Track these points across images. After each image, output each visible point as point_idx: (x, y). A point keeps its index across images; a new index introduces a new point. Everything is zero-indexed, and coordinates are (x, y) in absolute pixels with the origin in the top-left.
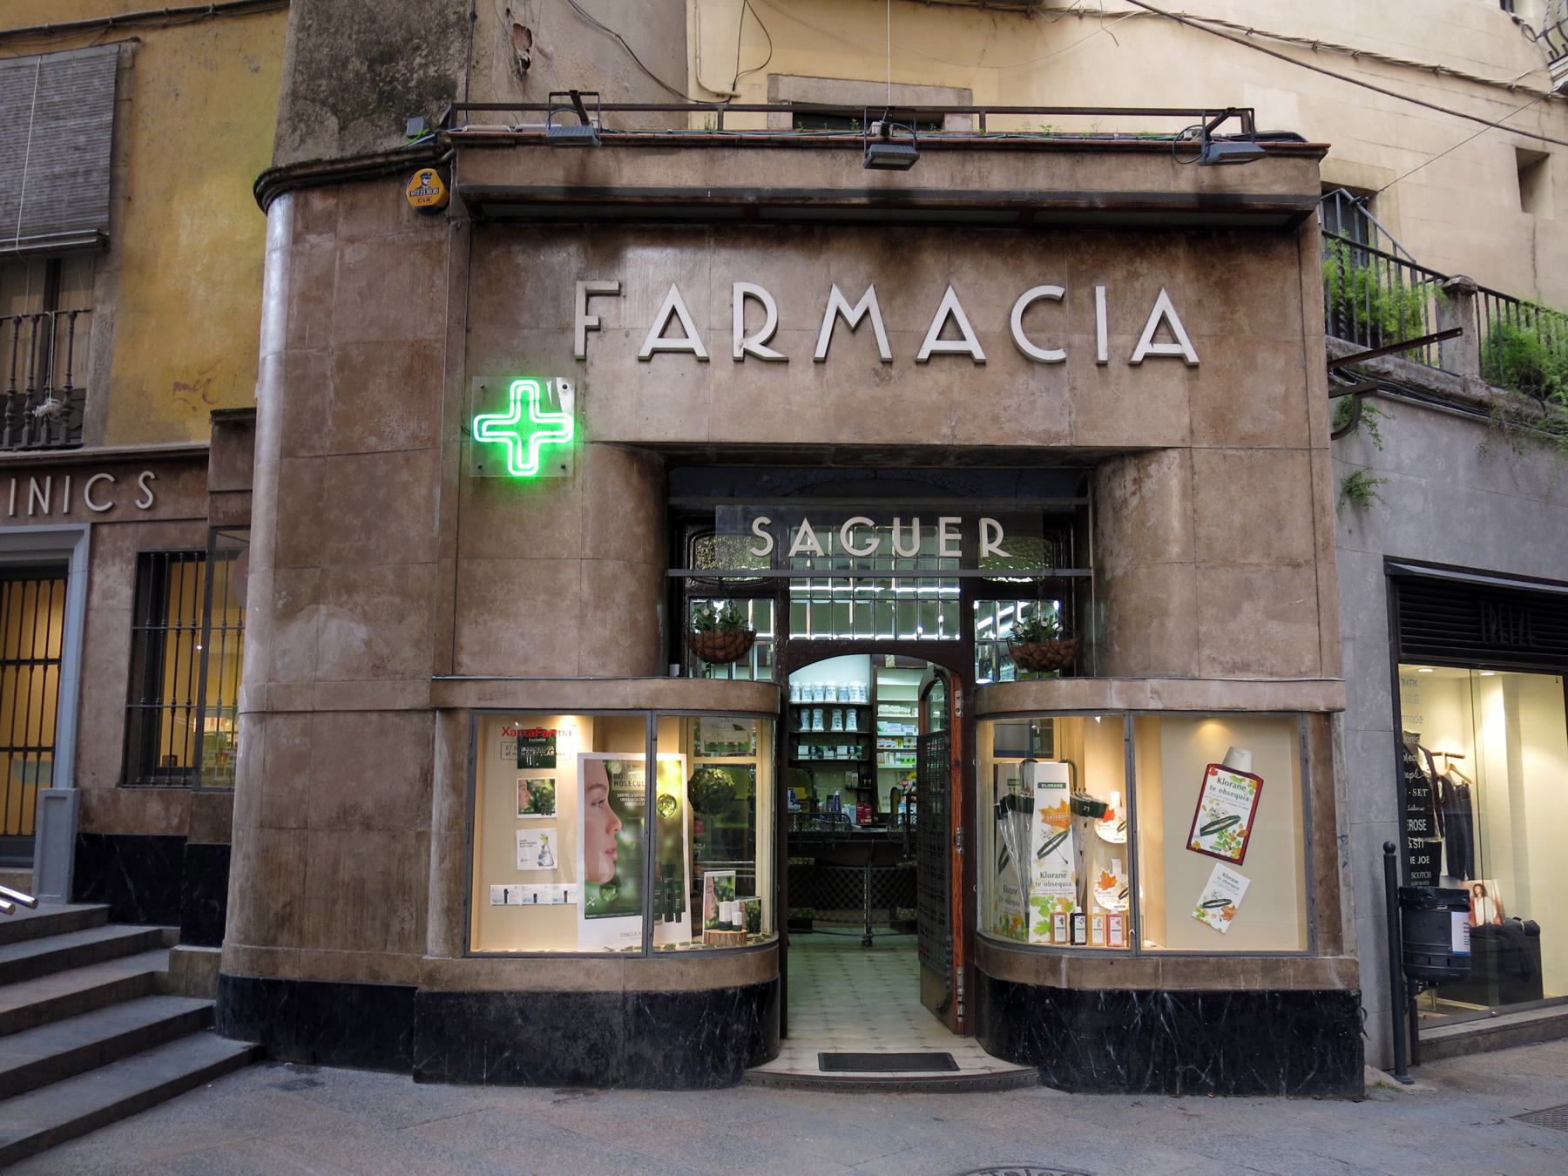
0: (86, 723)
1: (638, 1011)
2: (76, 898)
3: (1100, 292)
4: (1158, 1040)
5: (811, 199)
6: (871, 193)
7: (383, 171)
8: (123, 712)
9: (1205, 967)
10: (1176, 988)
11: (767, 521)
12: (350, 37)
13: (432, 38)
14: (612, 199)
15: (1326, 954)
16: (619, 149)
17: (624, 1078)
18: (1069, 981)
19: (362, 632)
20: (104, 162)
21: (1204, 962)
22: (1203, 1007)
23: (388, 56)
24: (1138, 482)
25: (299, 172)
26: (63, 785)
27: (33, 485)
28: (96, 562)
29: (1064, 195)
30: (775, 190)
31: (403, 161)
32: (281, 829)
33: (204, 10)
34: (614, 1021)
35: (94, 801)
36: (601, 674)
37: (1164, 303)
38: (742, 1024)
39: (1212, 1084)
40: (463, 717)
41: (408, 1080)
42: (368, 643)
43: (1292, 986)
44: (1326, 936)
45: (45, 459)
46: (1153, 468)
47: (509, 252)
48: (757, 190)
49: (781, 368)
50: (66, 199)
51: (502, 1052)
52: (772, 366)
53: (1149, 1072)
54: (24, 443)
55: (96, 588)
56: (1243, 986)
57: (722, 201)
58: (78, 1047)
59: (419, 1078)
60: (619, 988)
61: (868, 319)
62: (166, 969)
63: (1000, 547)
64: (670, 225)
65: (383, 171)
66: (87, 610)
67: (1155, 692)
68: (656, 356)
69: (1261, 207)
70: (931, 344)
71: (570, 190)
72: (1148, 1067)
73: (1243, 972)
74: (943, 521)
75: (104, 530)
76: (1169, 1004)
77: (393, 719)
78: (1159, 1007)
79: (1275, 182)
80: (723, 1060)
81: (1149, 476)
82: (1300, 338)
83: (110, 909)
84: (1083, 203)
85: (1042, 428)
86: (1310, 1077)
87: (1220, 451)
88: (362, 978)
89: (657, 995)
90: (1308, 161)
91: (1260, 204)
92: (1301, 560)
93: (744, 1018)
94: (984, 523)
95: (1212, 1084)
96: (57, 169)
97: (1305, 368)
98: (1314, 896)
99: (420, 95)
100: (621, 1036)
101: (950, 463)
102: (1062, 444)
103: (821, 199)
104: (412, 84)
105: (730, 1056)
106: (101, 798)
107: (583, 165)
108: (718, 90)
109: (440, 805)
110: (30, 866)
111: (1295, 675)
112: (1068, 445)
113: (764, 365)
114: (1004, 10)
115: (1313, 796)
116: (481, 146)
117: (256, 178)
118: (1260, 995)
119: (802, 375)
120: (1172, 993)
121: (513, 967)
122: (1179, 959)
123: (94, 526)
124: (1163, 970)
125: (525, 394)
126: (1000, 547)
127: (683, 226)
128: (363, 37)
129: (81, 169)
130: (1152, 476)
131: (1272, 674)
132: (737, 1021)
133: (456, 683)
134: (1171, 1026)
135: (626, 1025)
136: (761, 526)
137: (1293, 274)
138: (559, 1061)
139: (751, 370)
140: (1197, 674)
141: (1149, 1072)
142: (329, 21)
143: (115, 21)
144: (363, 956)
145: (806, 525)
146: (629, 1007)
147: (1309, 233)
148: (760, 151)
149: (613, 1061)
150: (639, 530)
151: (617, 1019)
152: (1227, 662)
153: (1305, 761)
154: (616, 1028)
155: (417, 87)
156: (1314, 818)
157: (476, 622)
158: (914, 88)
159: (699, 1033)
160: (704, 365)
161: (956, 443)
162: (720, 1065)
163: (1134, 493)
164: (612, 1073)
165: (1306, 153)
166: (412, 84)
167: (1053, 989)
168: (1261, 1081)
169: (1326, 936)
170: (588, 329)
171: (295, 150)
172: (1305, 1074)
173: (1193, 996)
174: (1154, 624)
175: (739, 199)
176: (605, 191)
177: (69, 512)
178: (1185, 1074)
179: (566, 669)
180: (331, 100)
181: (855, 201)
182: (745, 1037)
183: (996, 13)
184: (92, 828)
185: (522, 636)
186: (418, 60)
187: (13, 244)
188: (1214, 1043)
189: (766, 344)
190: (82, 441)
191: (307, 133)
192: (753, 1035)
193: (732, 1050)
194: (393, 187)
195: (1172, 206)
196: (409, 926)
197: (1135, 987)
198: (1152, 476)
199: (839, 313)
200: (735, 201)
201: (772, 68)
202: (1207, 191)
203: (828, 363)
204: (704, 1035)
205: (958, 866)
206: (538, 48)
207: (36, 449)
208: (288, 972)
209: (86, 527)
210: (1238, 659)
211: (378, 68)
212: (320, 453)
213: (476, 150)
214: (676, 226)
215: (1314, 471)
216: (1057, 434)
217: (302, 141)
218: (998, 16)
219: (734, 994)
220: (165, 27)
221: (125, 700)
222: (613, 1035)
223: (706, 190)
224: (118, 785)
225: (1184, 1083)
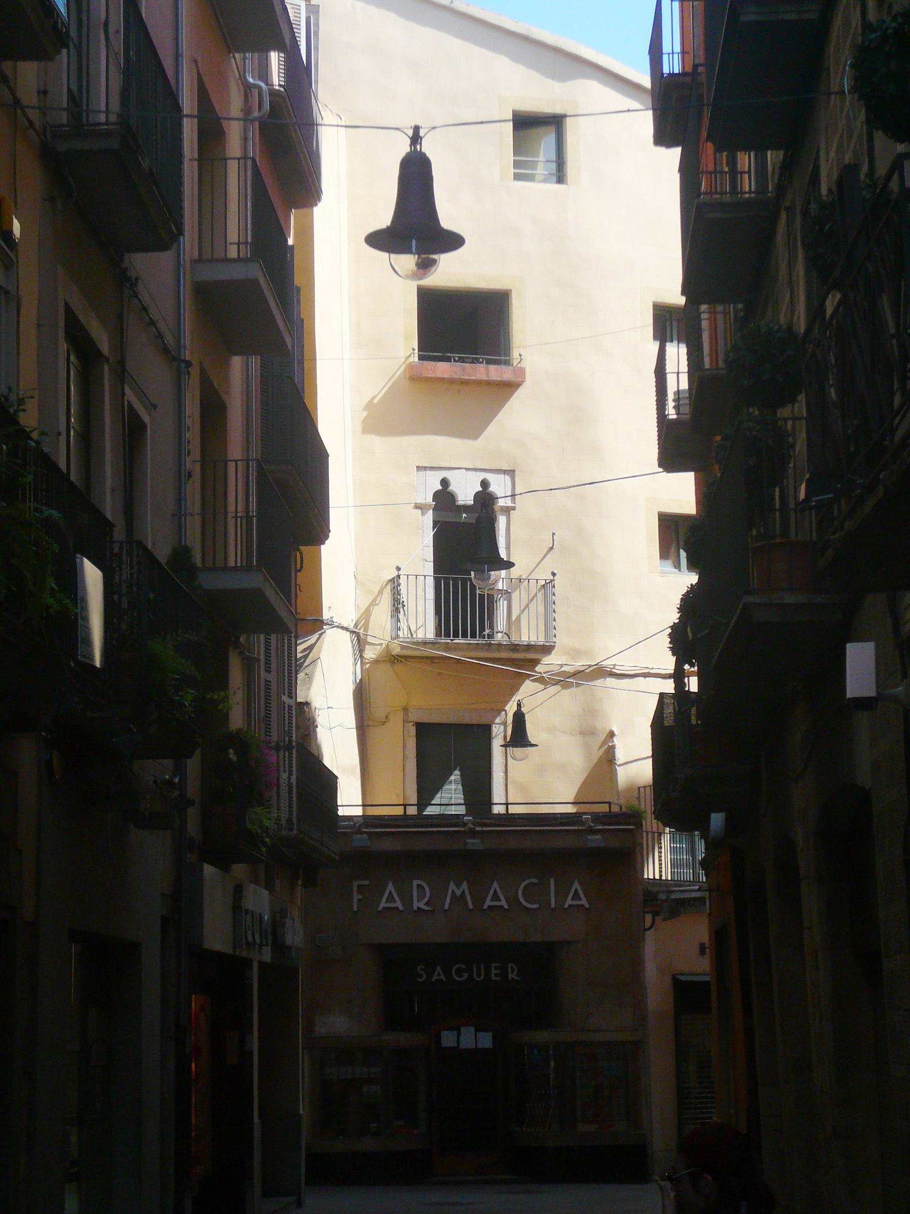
3: (552, 881)
37: (576, 885)
63: (516, 975)
70: (488, 903)
94: (510, 965)
117: (435, 273)
126: (516, 975)
189: (426, 904)
199: (453, 891)
205: (306, 639)
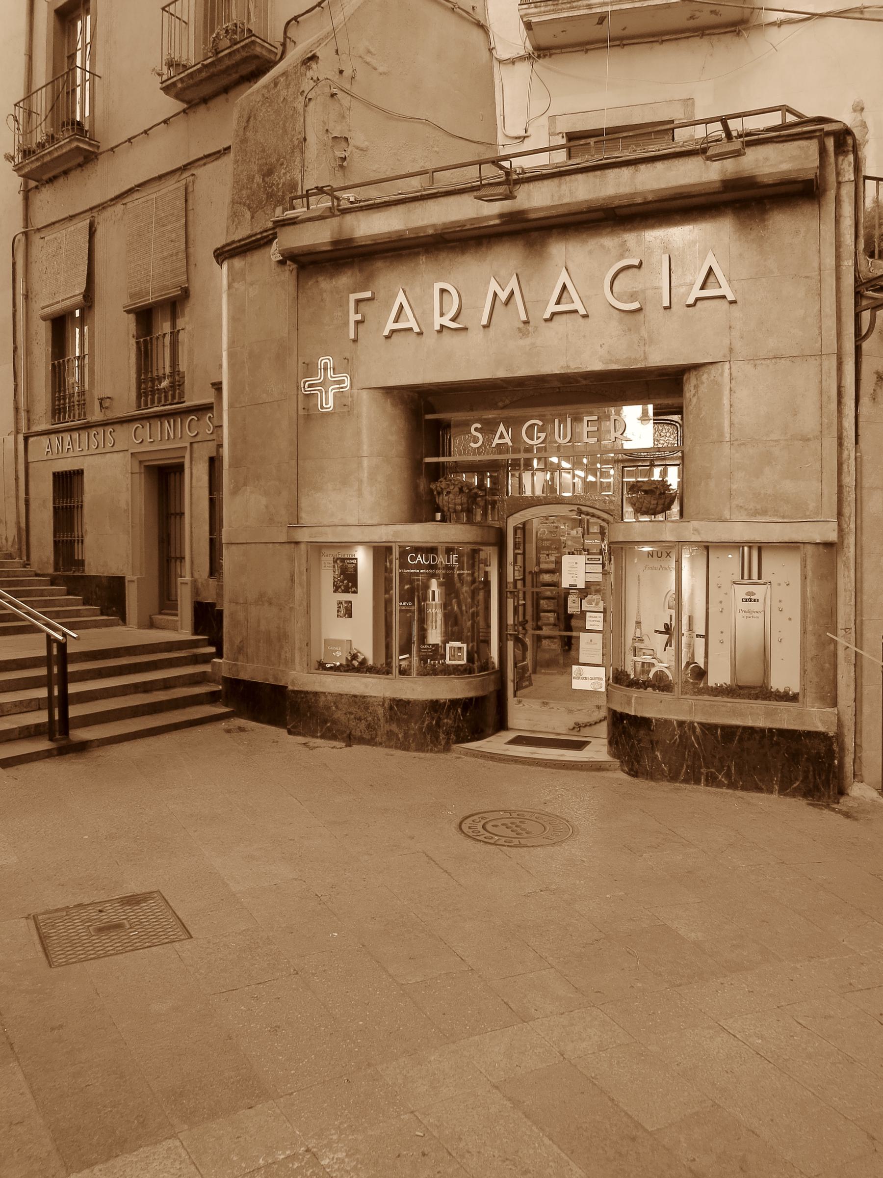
0: (195, 545)
1: (391, 708)
2: (196, 632)
4: (689, 751)
5: (465, 226)
6: (501, 216)
7: (262, 242)
8: (208, 540)
9: (724, 709)
10: (704, 721)
11: (479, 426)
12: (255, 163)
13: (288, 157)
14: (356, 244)
15: (813, 707)
16: (358, 213)
17: (385, 742)
18: (635, 711)
19: (264, 501)
20: (183, 247)
21: (723, 706)
22: (721, 734)
23: (270, 172)
24: (696, 387)
25: (228, 248)
26: (188, 578)
27: (167, 424)
28: (193, 462)
29: (626, 196)
30: (444, 224)
31: (268, 236)
32: (237, 603)
33: (219, 152)
34: (379, 712)
35: (200, 585)
36: (370, 522)
38: (450, 719)
39: (726, 782)
40: (303, 547)
41: (284, 732)
42: (267, 507)
43: (786, 726)
44: (814, 695)
45: (175, 409)
46: (705, 377)
47: (317, 282)
48: (434, 225)
49: (463, 333)
50: (169, 270)
51: (326, 723)
52: (458, 332)
53: (684, 770)
54: (163, 403)
55: (194, 475)
56: (750, 723)
57: (415, 236)
58: (84, 704)
59: (290, 732)
60: (381, 695)
61: (497, 298)
62: (210, 670)
64: (400, 252)
65: (262, 242)
66: (191, 487)
67: (696, 530)
68: (394, 334)
69: (770, 182)
71: (335, 243)
72: (682, 767)
73: (751, 714)
74: (586, 419)
75: (195, 445)
76: (698, 730)
77: (278, 546)
78: (691, 732)
79: (781, 162)
80: (437, 738)
81: (703, 383)
82: (817, 273)
83: (209, 639)
84: (639, 200)
85: (625, 356)
86: (795, 785)
87: (752, 362)
88: (271, 681)
89: (401, 700)
90: (809, 141)
91: (770, 181)
92: (809, 436)
93: (452, 716)
95: (726, 782)
96: (165, 254)
97: (820, 295)
98: (806, 668)
99: (283, 192)
100: (382, 720)
101: (556, 384)
102: (639, 366)
103: (472, 225)
104: (280, 186)
105: (442, 736)
106: (202, 584)
107: (340, 226)
108: (516, 135)
109: (298, 592)
110: (176, 615)
111: (801, 518)
112: (643, 366)
113: (454, 332)
114: (719, 34)
115: (809, 601)
116: (289, 224)
118: (762, 730)
119: (476, 336)
120: (700, 723)
121: (330, 680)
122: (707, 703)
123: (191, 444)
124: (695, 709)
125: (326, 364)
127: (407, 251)
128: (260, 162)
129: (174, 251)
130: (704, 383)
131: (783, 517)
132: (447, 718)
133: (298, 528)
134: (699, 744)
135: (385, 715)
136: (476, 429)
137: (814, 224)
138: (353, 731)
139: (447, 339)
140: (728, 517)
141: (684, 770)
142: (246, 155)
143: (184, 166)
144: (271, 669)
145: (502, 428)
146: (386, 705)
147: (828, 193)
148: (435, 200)
149: (379, 733)
150: (393, 438)
151: (380, 711)
152: (751, 509)
153: (804, 577)
154: (380, 716)
155: (282, 187)
156: (809, 616)
157: (308, 495)
158: (651, 105)
159: (423, 722)
160: (421, 336)
161: (569, 371)
162: (436, 740)
163: (694, 395)
164: (378, 739)
165: (806, 136)
166: (280, 186)
167: (628, 715)
168: (760, 784)
169: (814, 695)
170: (357, 323)
171: (234, 234)
172: (792, 782)
173: (715, 727)
174: (703, 484)
175: (425, 233)
176: (351, 240)
177: (181, 438)
178: (707, 774)
179: (352, 520)
180: (248, 202)
181: (492, 223)
182: (452, 727)
183: (713, 37)
184: (200, 599)
185: (330, 501)
186: (283, 171)
187: (149, 300)
188: (728, 757)
190: (185, 399)
191: (239, 223)
192: (458, 726)
193: (444, 733)
194: (267, 249)
195: (703, 192)
196: (289, 655)
197: (676, 718)
198: (704, 383)
200: (422, 234)
201: (551, 113)
202: (729, 176)
203: (491, 327)
204: (425, 725)
206: (354, 146)
207: (167, 405)
208: (244, 676)
209: (188, 445)
210: (759, 507)
211: (266, 179)
212: (243, 405)
213: (287, 228)
214: (404, 252)
215: (823, 371)
216: (635, 359)
217: (237, 228)
218: (714, 38)
219: (445, 703)
220: (205, 164)
221: (208, 534)
222: (379, 720)
223: (405, 230)
224: (208, 577)
225: (707, 780)
